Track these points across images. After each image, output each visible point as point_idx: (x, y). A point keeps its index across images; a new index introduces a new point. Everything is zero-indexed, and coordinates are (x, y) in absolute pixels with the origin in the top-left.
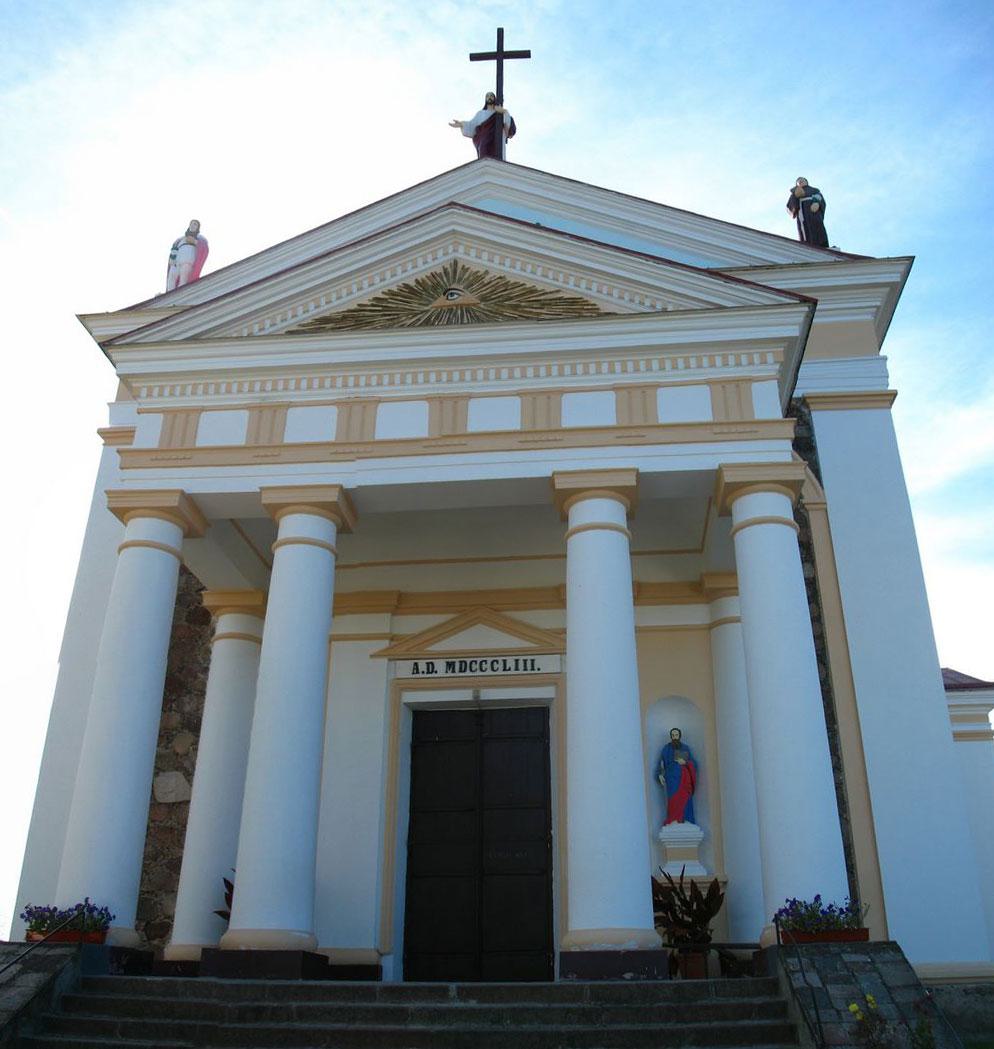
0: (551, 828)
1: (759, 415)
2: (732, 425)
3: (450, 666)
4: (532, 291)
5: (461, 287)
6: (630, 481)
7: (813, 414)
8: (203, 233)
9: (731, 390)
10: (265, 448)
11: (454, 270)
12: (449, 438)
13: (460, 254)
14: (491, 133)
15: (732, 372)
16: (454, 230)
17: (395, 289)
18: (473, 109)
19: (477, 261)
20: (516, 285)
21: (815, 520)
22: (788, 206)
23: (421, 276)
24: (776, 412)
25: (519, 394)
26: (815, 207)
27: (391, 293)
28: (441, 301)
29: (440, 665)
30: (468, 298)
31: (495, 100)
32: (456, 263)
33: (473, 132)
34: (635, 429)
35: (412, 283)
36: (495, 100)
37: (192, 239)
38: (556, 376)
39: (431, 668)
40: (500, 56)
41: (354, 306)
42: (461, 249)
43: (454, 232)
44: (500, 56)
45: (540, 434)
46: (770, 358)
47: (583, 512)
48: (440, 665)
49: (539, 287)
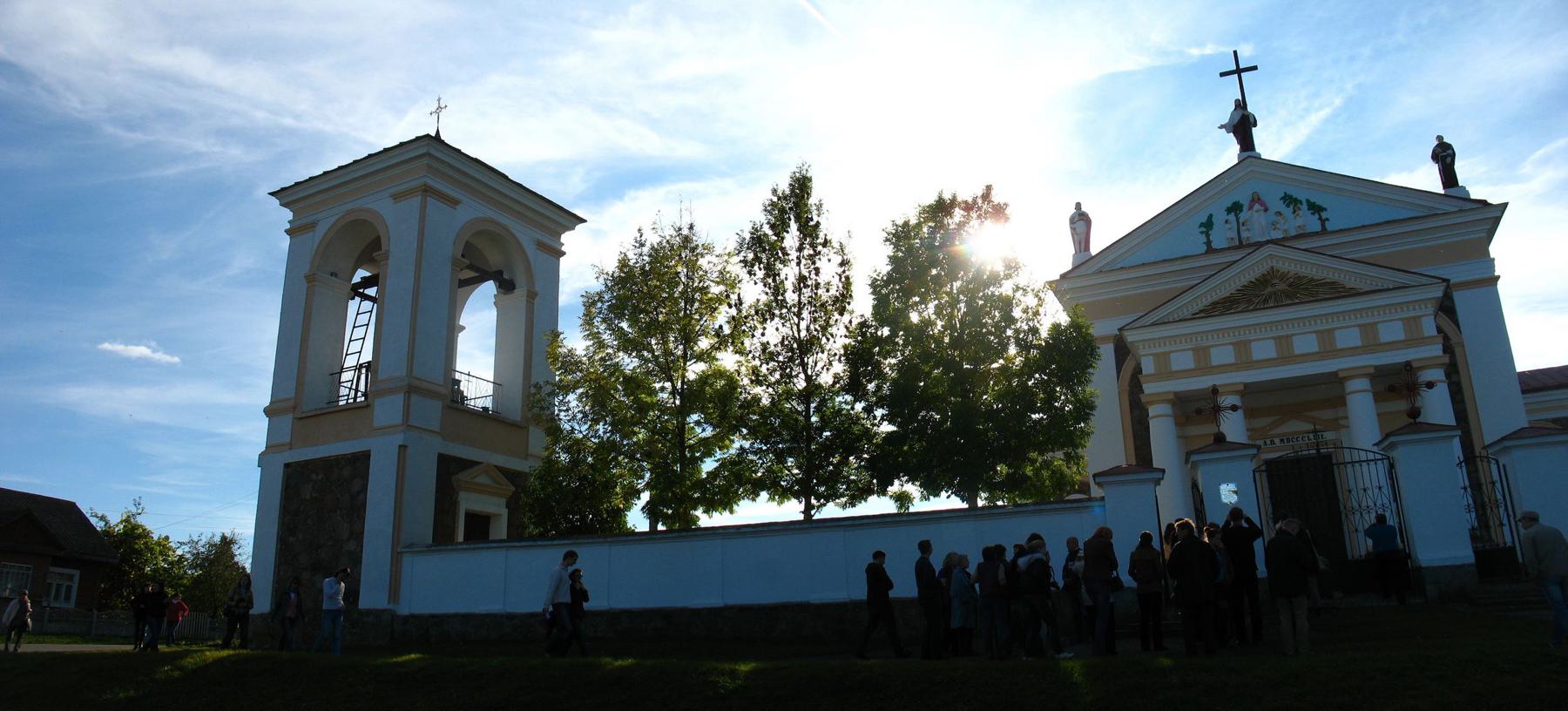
0: (68, 510)
1: (1426, 334)
2: (1415, 340)
3: (1282, 440)
4: (1312, 280)
5: (1277, 281)
6: (1372, 371)
7: (1454, 294)
8: (1083, 209)
9: (1412, 323)
10: (1203, 366)
11: (1273, 273)
12: (1286, 357)
13: (1274, 264)
14: (1242, 126)
15: (1412, 314)
16: (1392, 443)
17: (1246, 284)
18: (1226, 112)
19: (1283, 267)
20: (1304, 277)
21: (1458, 351)
22: (1432, 158)
23: (1257, 276)
24: (1434, 332)
25: (1314, 332)
26: (1449, 160)
27: (1245, 286)
28: (1269, 289)
29: (1277, 441)
30: (1282, 286)
31: (1241, 105)
32: (1272, 267)
33: (1232, 129)
34: (1371, 345)
35: (1253, 280)
36: (1241, 105)
37: (1082, 217)
38: (1355, 374)
39: (1272, 442)
40: (1239, 71)
41: (1228, 295)
42: (1274, 261)
43: (1271, 255)
44: (1239, 71)
45: (1328, 352)
46: (1429, 306)
47: (1353, 385)
48: (1277, 441)
49: (1315, 278)
